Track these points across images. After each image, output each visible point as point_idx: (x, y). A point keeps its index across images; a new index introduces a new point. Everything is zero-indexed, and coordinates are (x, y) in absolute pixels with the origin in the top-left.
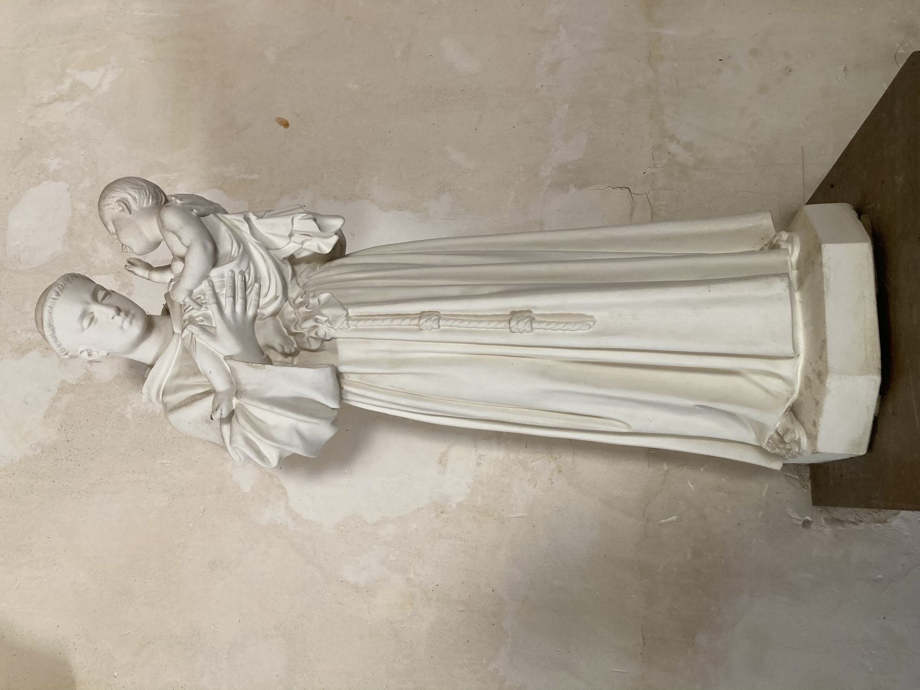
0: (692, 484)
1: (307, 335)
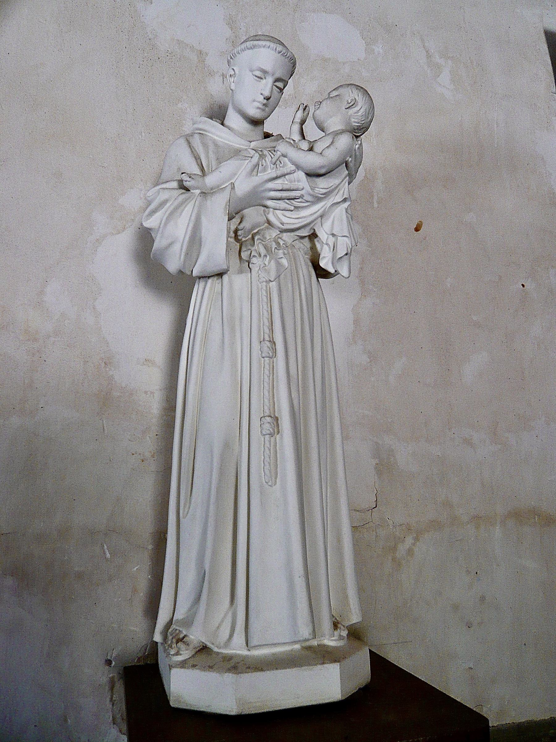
0: (137, 569)
1: (253, 249)
